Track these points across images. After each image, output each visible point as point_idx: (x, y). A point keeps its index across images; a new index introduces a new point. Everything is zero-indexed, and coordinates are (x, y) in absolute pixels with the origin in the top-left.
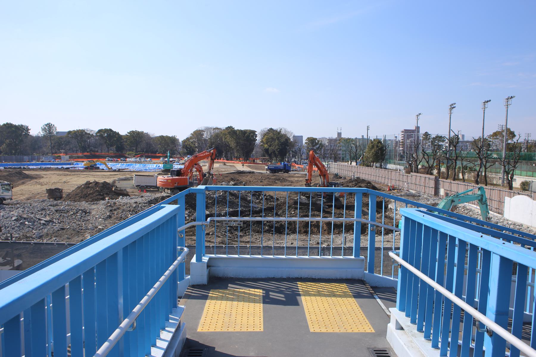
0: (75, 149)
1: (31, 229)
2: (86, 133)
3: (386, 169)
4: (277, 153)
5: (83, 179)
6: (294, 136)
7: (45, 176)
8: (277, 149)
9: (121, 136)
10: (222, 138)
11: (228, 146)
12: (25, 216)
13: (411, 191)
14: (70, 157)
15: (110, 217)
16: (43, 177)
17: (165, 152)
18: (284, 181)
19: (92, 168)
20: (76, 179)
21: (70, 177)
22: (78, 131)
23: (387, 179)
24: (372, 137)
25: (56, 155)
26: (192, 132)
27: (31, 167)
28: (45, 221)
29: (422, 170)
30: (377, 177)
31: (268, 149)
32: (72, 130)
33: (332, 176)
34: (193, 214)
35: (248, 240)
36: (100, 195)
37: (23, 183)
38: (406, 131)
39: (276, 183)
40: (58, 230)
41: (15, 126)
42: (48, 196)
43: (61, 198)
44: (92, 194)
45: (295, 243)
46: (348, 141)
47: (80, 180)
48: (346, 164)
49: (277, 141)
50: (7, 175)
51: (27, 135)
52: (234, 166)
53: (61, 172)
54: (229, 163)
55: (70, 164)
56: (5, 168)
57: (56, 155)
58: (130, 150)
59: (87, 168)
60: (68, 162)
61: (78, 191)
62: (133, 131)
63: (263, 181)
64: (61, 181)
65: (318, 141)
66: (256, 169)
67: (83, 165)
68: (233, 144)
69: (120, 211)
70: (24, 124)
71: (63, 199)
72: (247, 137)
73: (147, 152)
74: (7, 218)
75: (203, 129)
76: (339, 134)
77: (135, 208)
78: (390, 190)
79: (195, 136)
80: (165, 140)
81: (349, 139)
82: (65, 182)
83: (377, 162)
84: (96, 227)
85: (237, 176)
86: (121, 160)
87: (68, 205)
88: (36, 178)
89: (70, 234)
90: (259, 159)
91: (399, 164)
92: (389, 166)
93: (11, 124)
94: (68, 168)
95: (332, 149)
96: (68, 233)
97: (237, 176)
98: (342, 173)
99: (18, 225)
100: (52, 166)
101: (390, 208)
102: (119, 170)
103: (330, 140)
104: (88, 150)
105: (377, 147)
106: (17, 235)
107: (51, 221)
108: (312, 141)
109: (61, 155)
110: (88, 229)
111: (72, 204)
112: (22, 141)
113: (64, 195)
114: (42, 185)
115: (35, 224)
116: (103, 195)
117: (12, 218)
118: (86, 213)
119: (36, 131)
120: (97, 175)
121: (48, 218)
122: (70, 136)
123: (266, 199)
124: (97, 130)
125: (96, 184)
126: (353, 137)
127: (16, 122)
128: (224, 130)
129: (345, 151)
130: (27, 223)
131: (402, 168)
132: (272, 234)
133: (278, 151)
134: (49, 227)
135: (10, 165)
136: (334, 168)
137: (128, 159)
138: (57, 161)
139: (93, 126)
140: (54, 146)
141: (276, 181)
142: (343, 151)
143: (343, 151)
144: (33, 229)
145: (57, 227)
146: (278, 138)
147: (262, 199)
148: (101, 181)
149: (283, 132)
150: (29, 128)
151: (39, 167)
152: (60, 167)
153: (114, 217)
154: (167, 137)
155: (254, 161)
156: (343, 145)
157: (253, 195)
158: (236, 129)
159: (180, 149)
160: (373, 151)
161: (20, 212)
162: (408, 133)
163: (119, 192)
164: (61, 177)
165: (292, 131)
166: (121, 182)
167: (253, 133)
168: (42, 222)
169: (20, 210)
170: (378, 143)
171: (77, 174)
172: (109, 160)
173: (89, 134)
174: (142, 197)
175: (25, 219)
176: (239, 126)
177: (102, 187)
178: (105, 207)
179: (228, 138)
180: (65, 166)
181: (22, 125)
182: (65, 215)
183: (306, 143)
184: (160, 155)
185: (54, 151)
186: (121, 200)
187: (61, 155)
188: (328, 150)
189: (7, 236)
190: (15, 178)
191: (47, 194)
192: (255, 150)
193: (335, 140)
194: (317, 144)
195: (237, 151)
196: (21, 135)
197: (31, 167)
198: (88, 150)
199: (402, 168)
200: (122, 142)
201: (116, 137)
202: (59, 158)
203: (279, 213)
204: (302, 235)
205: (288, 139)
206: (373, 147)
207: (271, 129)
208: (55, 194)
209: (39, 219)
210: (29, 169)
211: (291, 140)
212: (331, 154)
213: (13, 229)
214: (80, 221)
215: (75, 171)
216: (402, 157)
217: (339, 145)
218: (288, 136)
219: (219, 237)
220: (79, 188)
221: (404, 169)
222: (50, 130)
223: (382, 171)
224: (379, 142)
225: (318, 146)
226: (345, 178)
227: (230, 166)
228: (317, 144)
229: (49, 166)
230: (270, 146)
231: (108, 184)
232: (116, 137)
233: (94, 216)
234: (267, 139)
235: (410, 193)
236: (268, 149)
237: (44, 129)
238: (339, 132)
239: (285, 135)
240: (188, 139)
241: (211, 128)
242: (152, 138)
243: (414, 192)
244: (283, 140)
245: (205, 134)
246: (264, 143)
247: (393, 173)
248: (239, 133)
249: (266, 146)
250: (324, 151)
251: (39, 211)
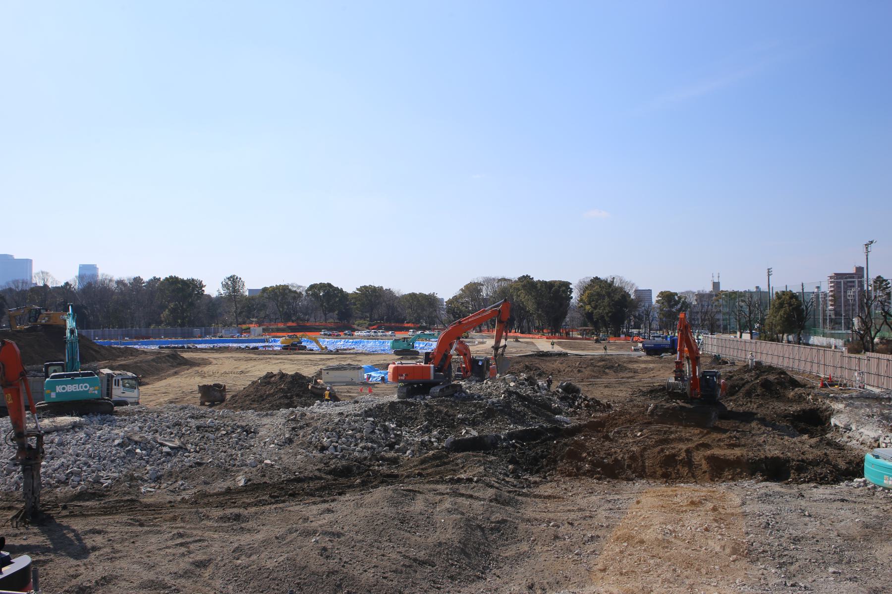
0: (272, 316)
2: (290, 290)
3: (808, 344)
4: (607, 319)
6: (636, 291)
7: (214, 362)
8: (607, 314)
9: (347, 294)
10: (512, 296)
11: (523, 308)
12: (136, 438)
13: (869, 388)
14: (264, 330)
15: (290, 441)
16: (210, 363)
17: (417, 321)
18: (621, 370)
19: (293, 348)
21: (253, 363)
22: (278, 287)
23: (815, 366)
24: (778, 285)
25: (244, 327)
26: (462, 287)
27: (199, 346)
28: (171, 448)
29: (880, 346)
30: (797, 362)
31: (592, 313)
33: (709, 360)
34: (446, 437)
35: (549, 492)
36: (286, 397)
37: (176, 373)
38: (838, 276)
39: (607, 374)
40: (191, 466)
41: (183, 281)
43: (222, 400)
44: (272, 395)
45: (644, 501)
46: (733, 296)
47: (259, 369)
48: (732, 336)
49: (607, 299)
50: (153, 360)
51: (201, 294)
52: (532, 343)
53: (242, 355)
54: (525, 339)
56: (160, 348)
57: (244, 327)
58: (361, 318)
59: (285, 348)
60: (260, 338)
61: (252, 389)
62: (365, 287)
63: (583, 370)
64: (236, 370)
65: (680, 298)
66: (572, 347)
67: (279, 344)
68: (530, 306)
69: (309, 430)
70: (195, 278)
71: (224, 404)
73: (388, 320)
74: (106, 441)
75: (480, 280)
76: (716, 285)
77: (337, 424)
78: (824, 386)
79: (468, 293)
80: (418, 301)
81: (734, 293)
82: (242, 372)
83: (790, 333)
84: (261, 462)
85: (537, 361)
86: (345, 334)
88: (198, 365)
89: (210, 474)
90: (577, 330)
91: (832, 336)
92: (815, 340)
93: (176, 278)
94: (256, 348)
95: (704, 310)
96: (208, 471)
97: (537, 362)
98: (728, 354)
99: (123, 454)
100: (231, 345)
101: (836, 425)
102: (337, 352)
103: (701, 296)
104: (294, 318)
105: (790, 305)
106: (116, 475)
107: (181, 448)
108: (668, 298)
110: (246, 465)
112: (192, 304)
113: (228, 397)
114: (204, 377)
115: (153, 452)
116: (291, 397)
117: (113, 441)
118: (248, 432)
119: (213, 289)
120: (298, 360)
121: (177, 443)
122: (265, 295)
123: (587, 406)
125: (281, 378)
126: (741, 289)
127: (184, 275)
128: (515, 281)
129: (728, 313)
130: (138, 451)
131: (840, 342)
132: (599, 479)
133: (610, 317)
135: (172, 343)
136: (710, 344)
137: (356, 333)
138: (245, 336)
139: (301, 277)
140: (241, 313)
141: (607, 371)
142: (724, 314)
143: (724, 314)
144: (147, 462)
145: (190, 459)
146: (609, 294)
147: (579, 406)
149: (617, 284)
151: (211, 346)
152: (243, 346)
153: (297, 441)
154: (422, 295)
155: (567, 334)
156: (724, 303)
157: (562, 399)
158: (535, 279)
159: (444, 315)
160: (782, 312)
162: (841, 281)
163: (318, 391)
164: (238, 363)
165: (633, 282)
166: (331, 372)
167: (566, 286)
168: (166, 449)
172: (325, 334)
173: (295, 292)
174: (356, 402)
175: (136, 443)
176: (540, 275)
177: (291, 382)
179: (522, 295)
180: (252, 345)
181: (193, 280)
182: (212, 436)
183: (658, 302)
184: (409, 325)
185: (240, 320)
186: (318, 408)
187: (252, 326)
188: (697, 313)
189: (98, 476)
190: (164, 365)
193: (710, 295)
194: (677, 303)
195: (539, 316)
196: (190, 295)
197: (199, 346)
198: (294, 318)
199: (840, 342)
200: (347, 305)
201: (337, 296)
202: (248, 331)
203: (611, 435)
204: (658, 482)
205: (626, 295)
206: (781, 305)
207: (597, 278)
208: (213, 395)
209: (162, 445)
210: (197, 350)
211: (632, 297)
212: (703, 320)
213: (113, 461)
215: (269, 353)
216: (835, 323)
217: (716, 303)
218: (627, 289)
219: (492, 486)
221: (845, 345)
222: (234, 287)
223: (804, 351)
224: (793, 296)
225: (679, 306)
226: (733, 364)
227: (527, 343)
228: (677, 303)
229: (221, 345)
230: (595, 308)
231: (304, 377)
232: (337, 296)
234: (590, 296)
235: (869, 394)
236: (592, 313)
237: (225, 286)
238: (716, 281)
239: (621, 289)
240: (455, 299)
241: (494, 279)
242: (397, 298)
243: (877, 391)
244: (617, 297)
245: (484, 288)
246: (584, 303)
247: (829, 354)
248: (541, 286)
249: (588, 307)
250: (690, 316)
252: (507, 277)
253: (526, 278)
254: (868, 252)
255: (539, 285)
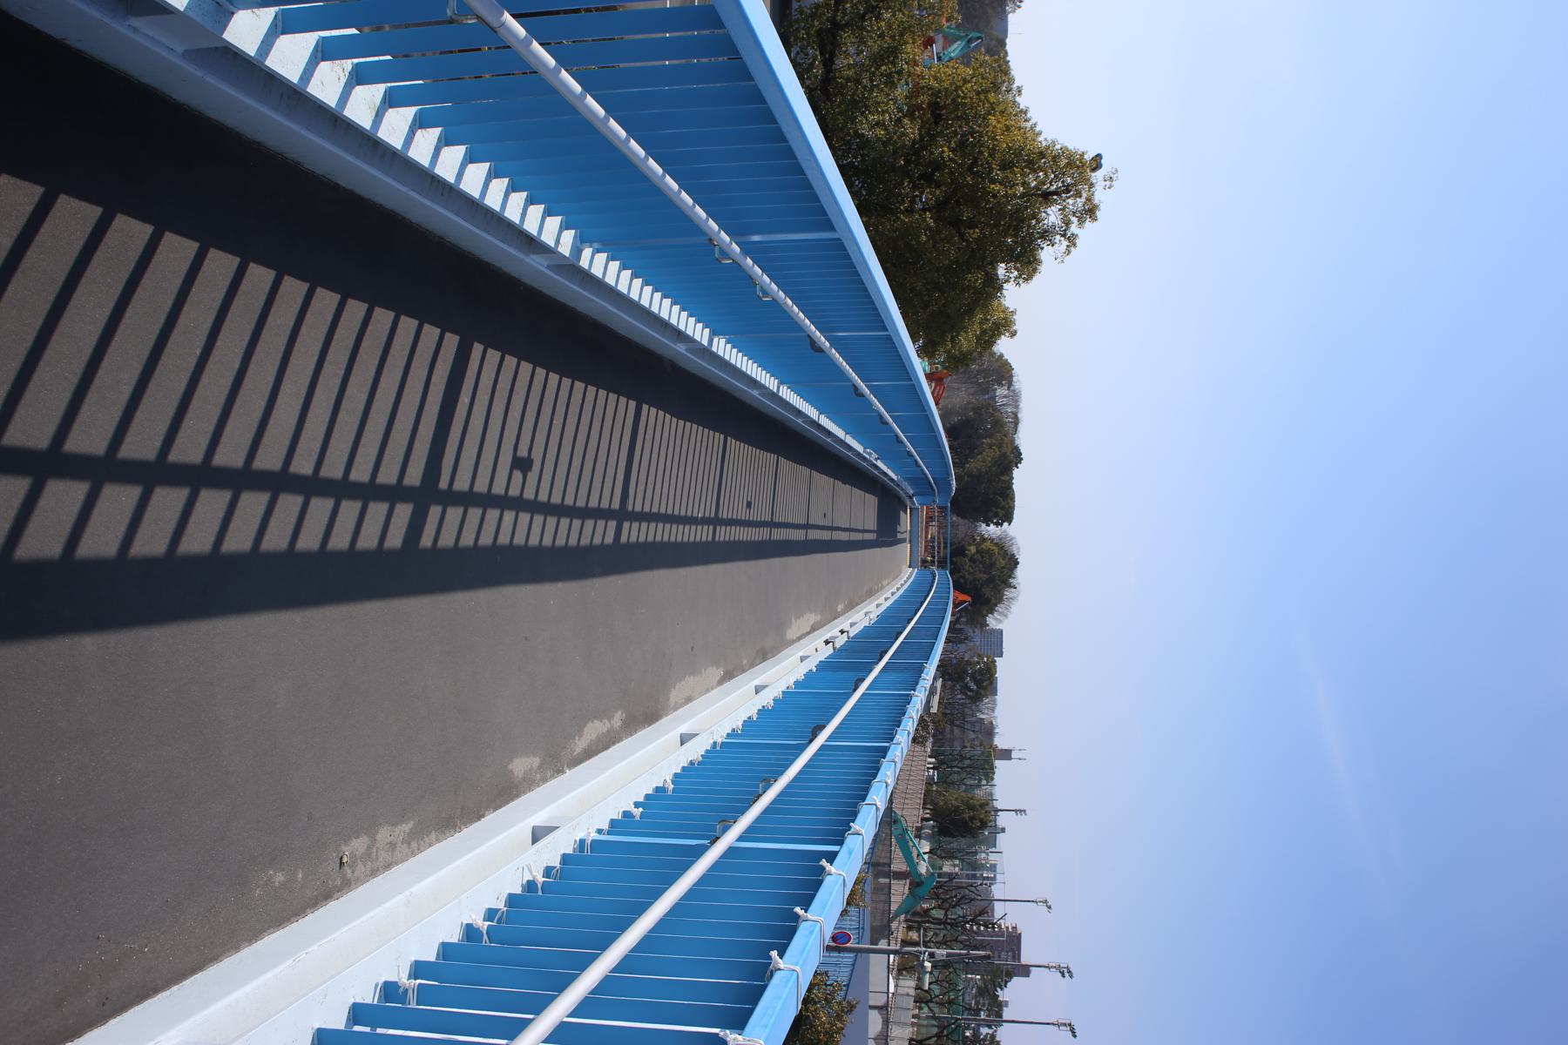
10: (991, 436)
49: (984, 577)
72: (999, 504)
75: (1016, 386)
76: (1006, 754)
79: (996, 365)
103: (989, 731)
105: (972, 818)
124: (740, 724)
128: (1013, 441)
146: (991, 580)
149: (1008, 593)
167: (1007, 516)
170: (981, 821)
176: (1021, 479)
181: (994, 692)
192: (961, 520)
206: (972, 808)
230: (972, 560)
234: (989, 552)
236: (965, 555)
239: (1000, 600)
241: (1017, 407)
244: (987, 592)
249: (973, 549)
252: (1021, 427)
253: (1017, 457)
254: (1058, 1025)
255: (1006, 478)
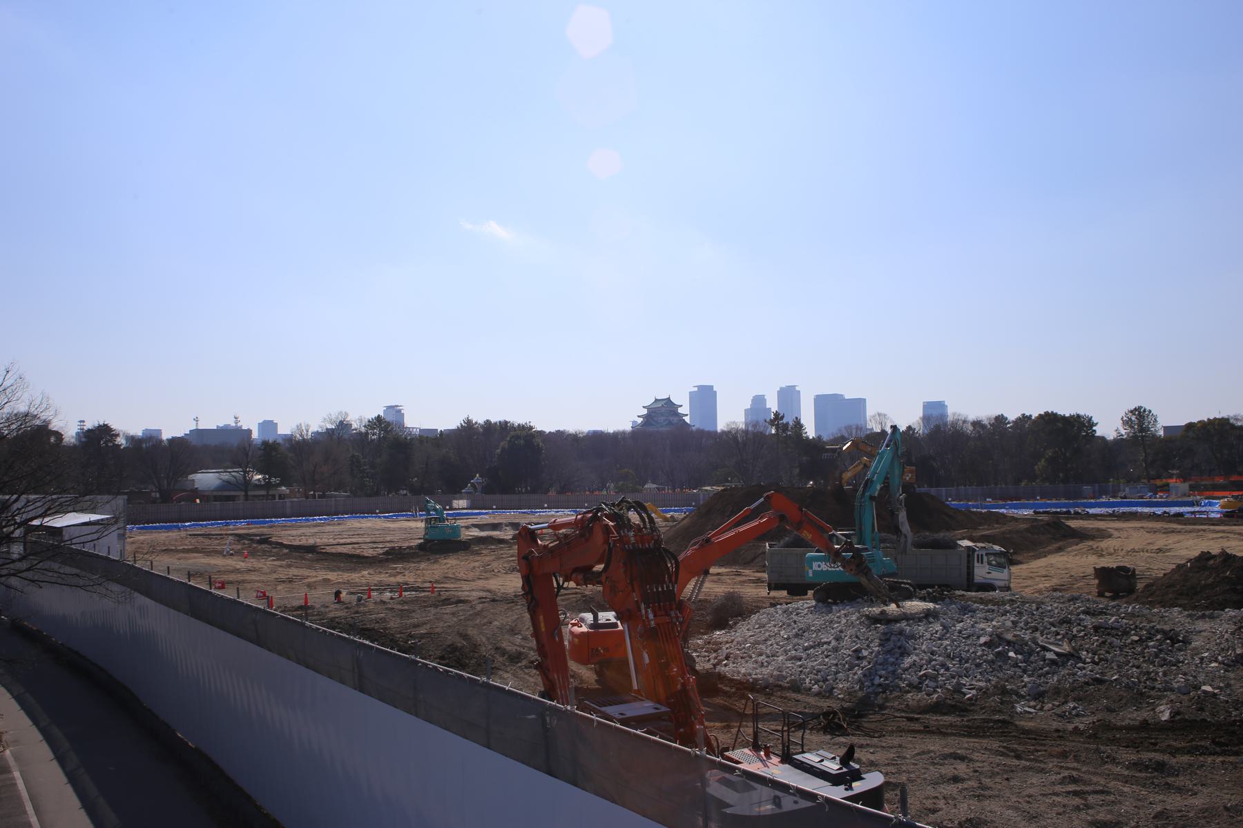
1: (1019, 672)
5: (1211, 543)
7: (1116, 534)
12: (1009, 637)
14: (1192, 488)
16: (1110, 536)
20: (1191, 542)
21: (1180, 537)
25: (1158, 483)
27: (1091, 511)
28: (1057, 654)
32: (1195, 420)
37: (1060, 549)
40: (1087, 683)
42: (1099, 585)
43: (1131, 590)
47: (1188, 547)
50: (1027, 530)
51: (1091, 437)
53: (1158, 525)
55: (1192, 504)
57: (1158, 483)
61: (1176, 576)
64: (1151, 547)
70: (1082, 413)
71: (1134, 596)
82: (1160, 550)
84: (1197, 688)
87: (1132, 615)
88: (1093, 538)
99: (991, 657)
100: (1139, 509)
106: (982, 684)
107: (1072, 655)
109: (1172, 482)
110: (1172, 690)
111: (1146, 612)
113: (1140, 586)
114: (1102, 555)
115: (1032, 658)
117: (978, 637)
118: (1174, 640)
119: (1109, 427)
121: (1065, 648)
122: (1191, 434)
127: (1065, 409)
130: (1011, 654)
134: (1064, 672)
144: (1025, 671)
145: (1085, 672)
148: (1215, 551)
150: (1095, 420)
151: (1110, 510)
152: (1159, 511)
161: (1009, 624)
168: (1050, 656)
169: (1008, 620)
171: (1199, 531)
175: (1009, 643)
178: (1232, 628)
181: (1078, 416)
182: (1117, 642)
187: (1172, 482)
189: (958, 684)
191: (1097, 581)
197: (1091, 511)
202: (1165, 488)
208: (1116, 582)
213: (979, 665)
214: (1153, 663)
220: (1179, 567)
222: (1141, 424)
233: (1196, 652)
237: (1127, 422)
251: (1053, 625)
